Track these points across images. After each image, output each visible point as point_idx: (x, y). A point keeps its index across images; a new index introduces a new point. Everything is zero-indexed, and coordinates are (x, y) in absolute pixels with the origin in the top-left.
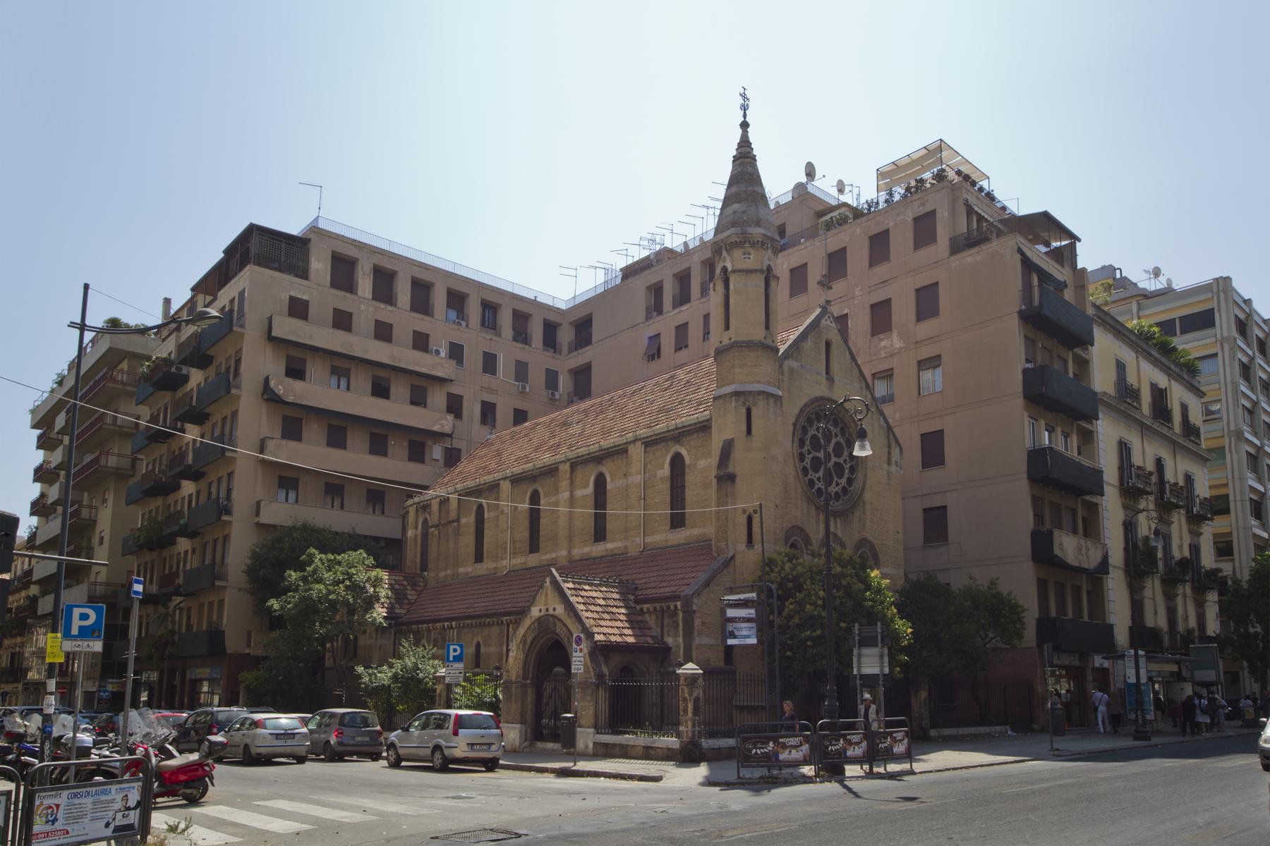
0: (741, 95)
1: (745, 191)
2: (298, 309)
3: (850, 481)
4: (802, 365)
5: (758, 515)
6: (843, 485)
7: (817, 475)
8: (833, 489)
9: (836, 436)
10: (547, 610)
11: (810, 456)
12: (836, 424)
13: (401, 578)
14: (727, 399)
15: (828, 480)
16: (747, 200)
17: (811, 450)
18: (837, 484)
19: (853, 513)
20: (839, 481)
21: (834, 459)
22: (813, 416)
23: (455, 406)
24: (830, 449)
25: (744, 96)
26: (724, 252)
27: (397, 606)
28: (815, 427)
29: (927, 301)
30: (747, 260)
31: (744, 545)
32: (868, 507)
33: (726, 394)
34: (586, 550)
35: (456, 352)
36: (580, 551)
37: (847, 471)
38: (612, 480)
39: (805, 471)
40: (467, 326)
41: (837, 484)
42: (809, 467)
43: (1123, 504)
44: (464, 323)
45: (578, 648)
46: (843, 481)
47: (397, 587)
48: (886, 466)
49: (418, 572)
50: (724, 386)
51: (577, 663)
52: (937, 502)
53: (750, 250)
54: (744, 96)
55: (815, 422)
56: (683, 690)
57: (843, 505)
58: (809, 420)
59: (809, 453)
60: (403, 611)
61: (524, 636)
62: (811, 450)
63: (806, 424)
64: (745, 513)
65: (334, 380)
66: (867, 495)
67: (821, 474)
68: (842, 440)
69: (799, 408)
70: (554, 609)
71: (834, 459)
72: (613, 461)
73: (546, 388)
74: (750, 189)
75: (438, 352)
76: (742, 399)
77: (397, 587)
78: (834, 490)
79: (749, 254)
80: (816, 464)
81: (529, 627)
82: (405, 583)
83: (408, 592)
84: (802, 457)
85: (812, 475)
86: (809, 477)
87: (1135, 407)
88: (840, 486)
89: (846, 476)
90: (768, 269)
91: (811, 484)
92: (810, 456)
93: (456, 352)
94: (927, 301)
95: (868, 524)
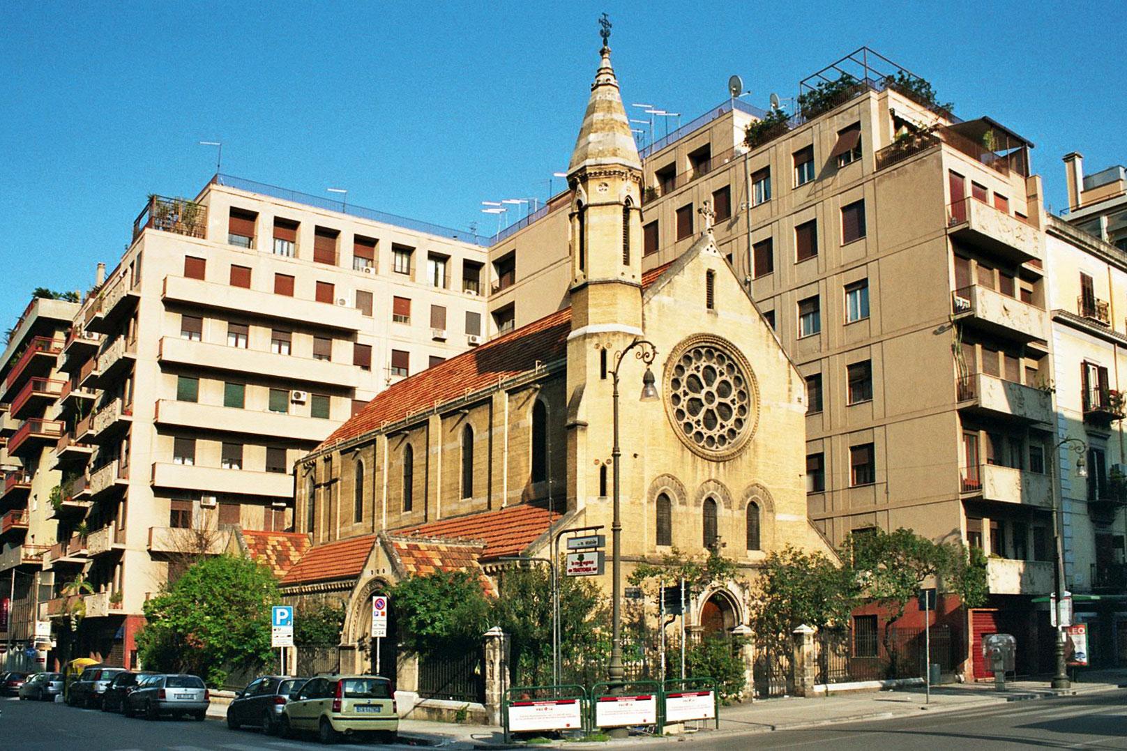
0: (600, 21)
1: (603, 120)
2: (195, 268)
3: (739, 422)
4: (675, 300)
5: (612, 465)
6: (730, 427)
7: (696, 419)
8: (716, 432)
9: (722, 374)
10: (378, 571)
11: (687, 398)
12: (721, 359)
13: (285, 539)
14: (581, 342)
15: (710, 421)
16: (603, 129)
17: (687, 391)
18: (722, 426)
19: (740, 456)
20: (724, 423)
21: (718, 400)
22: (691, 355)
23: (363, 358)
24: (714, 389)
25: (605, 23)
26: (580, 186)
27: (277, 567)
28: (693, 366)
29: (855, 219)
30: (603, 192)
31: (597, 497)
32: (761, 450)
33: (610, 332)
34: (455, 506)
35: (364, 301)
36: (449, 509)
37: (735, 412)
38: (478, 432)
39: (680, 414)
40: (376, 273)
41: (722, 426)
42: (685, 410)
43: (1086, 431)
44: (373, 270)
45: (380, 612)
46: (730, 423)
47: (279, 548)
48: (785, 405)
49: (306, 532)
50: (579, 328)
51: (378, 626)
52: (864, 439)
53: (606, 181)
54: (605, 23)
55: (694, 361)
56: (489, 652)
57: (727, 449)
58: (687, 359)
59: (686, 394)
60: (283, 573)
61: (358, 598)
62: (687, 391)
63: (682, 364)
64: (596, 464)
65: (232, 340)
66: (759, 437)
67: (701, 416)
68: (728, 379)
69: (673, 347)
70: (384, 571)
71: (718, 400)
72: (479, 412)
73: (467, 332)
74: (608, 116)
75: (343, 302)
76: (595, 340)
77: (279, 548)
78: (718, 434)
79: (606, 185)
80: (695, 406)
81: (363, 589)
82: (289, 544)
83: (291, 553)
84: (676, 398)
85: (688, 418)
86: (685, 420)
87: (1102, 324)
88: (726, 429)
89: (734, 417)
90: (627, 201)
91: (688, 426)
92: (687, 398)
93: (364, 301)
94: (855, 219)
95: (761, 467)
